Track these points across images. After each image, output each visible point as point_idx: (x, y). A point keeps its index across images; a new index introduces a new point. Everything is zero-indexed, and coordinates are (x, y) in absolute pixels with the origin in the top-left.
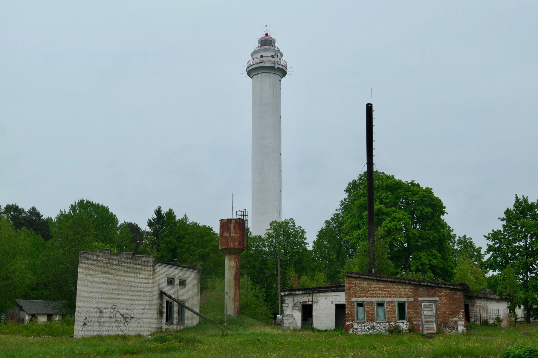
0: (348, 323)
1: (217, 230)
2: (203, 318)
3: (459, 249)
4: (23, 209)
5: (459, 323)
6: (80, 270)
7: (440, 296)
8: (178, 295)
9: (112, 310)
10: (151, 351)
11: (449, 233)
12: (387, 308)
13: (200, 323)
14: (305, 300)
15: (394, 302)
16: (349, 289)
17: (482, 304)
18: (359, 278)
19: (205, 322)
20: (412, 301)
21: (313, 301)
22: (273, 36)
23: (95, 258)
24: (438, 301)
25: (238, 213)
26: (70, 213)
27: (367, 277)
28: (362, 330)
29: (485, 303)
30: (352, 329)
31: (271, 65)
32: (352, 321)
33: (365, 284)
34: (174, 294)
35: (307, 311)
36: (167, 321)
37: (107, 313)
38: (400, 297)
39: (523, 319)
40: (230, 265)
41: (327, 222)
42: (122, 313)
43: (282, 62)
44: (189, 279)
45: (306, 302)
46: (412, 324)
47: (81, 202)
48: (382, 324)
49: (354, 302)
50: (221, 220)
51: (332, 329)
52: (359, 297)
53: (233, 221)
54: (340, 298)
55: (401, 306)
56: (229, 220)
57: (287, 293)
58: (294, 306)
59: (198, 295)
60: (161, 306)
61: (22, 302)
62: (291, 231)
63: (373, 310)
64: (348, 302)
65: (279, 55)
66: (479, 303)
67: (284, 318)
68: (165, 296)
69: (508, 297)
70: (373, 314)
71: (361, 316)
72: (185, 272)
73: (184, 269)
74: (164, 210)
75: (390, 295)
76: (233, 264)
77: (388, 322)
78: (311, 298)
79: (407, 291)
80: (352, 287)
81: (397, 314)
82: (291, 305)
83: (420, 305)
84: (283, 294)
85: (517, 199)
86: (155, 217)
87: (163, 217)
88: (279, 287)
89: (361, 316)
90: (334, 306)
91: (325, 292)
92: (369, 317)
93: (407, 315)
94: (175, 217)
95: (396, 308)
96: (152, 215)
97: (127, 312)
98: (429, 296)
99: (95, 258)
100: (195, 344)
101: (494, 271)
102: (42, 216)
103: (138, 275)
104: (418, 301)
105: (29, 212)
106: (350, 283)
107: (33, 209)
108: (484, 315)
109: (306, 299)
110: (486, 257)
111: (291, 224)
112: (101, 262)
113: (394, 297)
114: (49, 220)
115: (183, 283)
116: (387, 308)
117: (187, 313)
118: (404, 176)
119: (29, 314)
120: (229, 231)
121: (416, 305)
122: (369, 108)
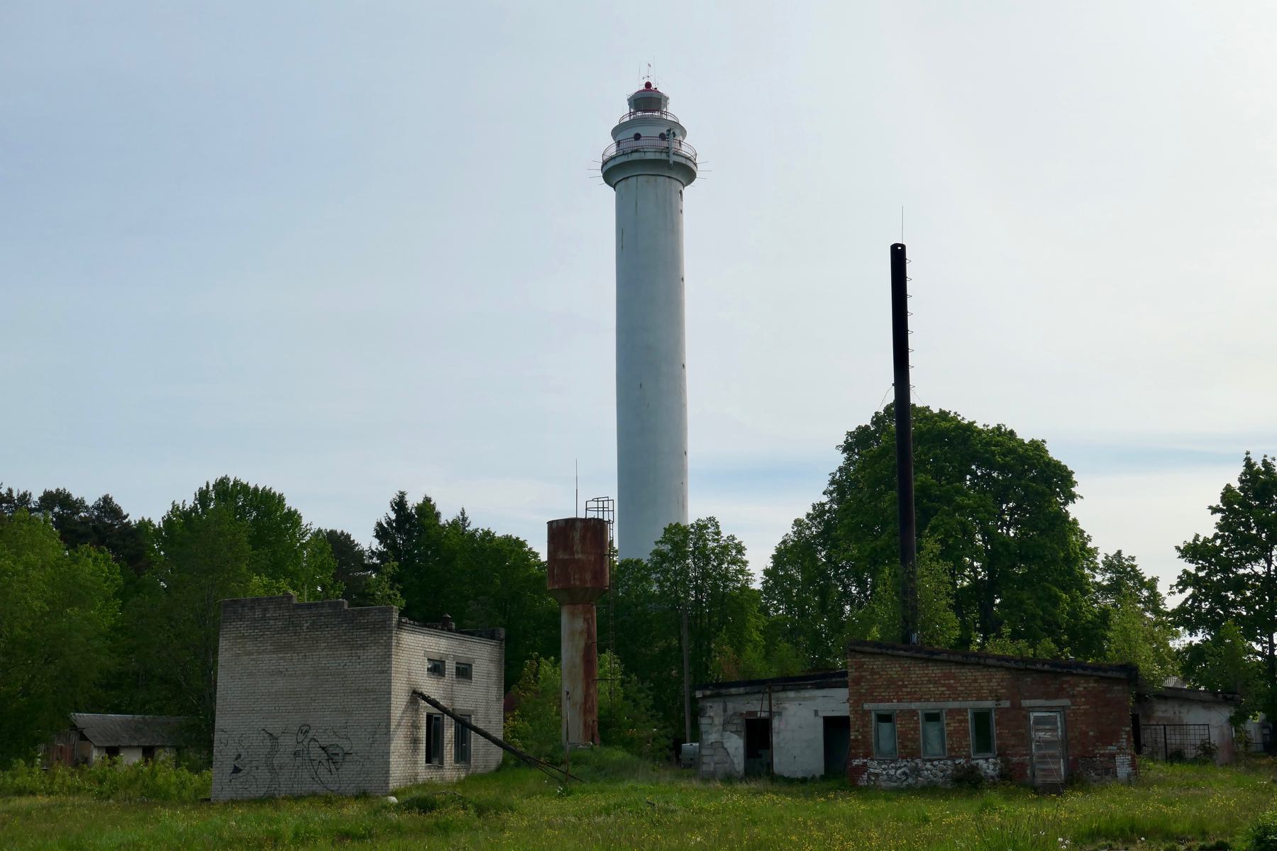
0: (856, 762)
1: (540, 547)
2: (514, 752)
3: (1105, 583)
4: (82, 502)
5: (1119, 759)
6: (223, 644)
7: (1073, 696)
8: (451, 699)
9: (301, 737)
10: (398, 830)
11: (1085, 544)
12: (948, 724)
13: (502, 767)
14: (752, 709)
15: (966, 710)
16: (858, 681)
17: (1170, 714)
18: (1001, 667)
19: (517, 758)
20: (1007, 709)
21: (770, 711)
22: (661, 87)
23: (258, 614)
24: (1068, 707)
25: (590, 505)
26: (194, 509)
27: (901, 652)
28: (890, 778)
29: (1177, 709)
30: (865, 777)
31: (658, 156)
32: (865, 756)
33: (894, 670)
34: (445, 698)
35: (758, 734)
36: (428, 760)
37: (288, 743)
38: (979, 699)
39: (1260, 747)
40: (573, 630)
41: (798, 523)
42: (324, 744)
43: (685, 150)
44: (477, 661)
45: (755, 713)
46: (1006, 762)
47: (222, 484)
48: (936, 763)
49: (870, 711)
50: (550, 524)
51: (817, 776)
52: (881, 701)
53: (579, 524)
54: (836, 702)
55: (982, 719)
56: (570, 523)
57: (708, 693)
58: (725, 724)
59: (498, 700)
60: (415, 726)
61: (83, 718)
62: (711, 545)
63: (916, 729)
64: (856, 712)
65: (677, 132)
66: (1162, 711)
67: (704, 752)
68: (423, 703)
69: (1229, 696)
70: (915, 740)
71: (886, 743)
72: (468, 644)
73: (467, 638)
74: (413, 501)
75: (956, 696)
76: (580, 624)
77: (950, 758)
78: (766, 703)
79: (994, 684)
80: (862, 677)
81: (971, 739)
82: (718, 721)
83: (1027, 718)
84: (699, 694)
85: (1249, 464)
86: (393, 516)
87: (410, 516)
88: (686, 678)
89: (886, 743)
90: (821, 721)
91: (798, 688)
92: (905, 747)
93: (996, 742)
94: (438, 515)
95: (970, 726)
96: (385, 513)
97: (335, 741)
98: (1047, 696)
99: (258, 614)
100: (504, 816)
101: (1193, 631)
102: (126, 517)
103: (360, 652)
104: (1021, 708)
105: (97, 507)
106: (860, 666)
107: (107, 500)
108: (1174, 740)
109: (756, 706)
110: (1172, 602)
111: (712, 530)
112: (272, 622)
113: (965, 699)
114: (144, 525)
115: (464, 672)
116: (950, 725)
117: (476, 742)
118: (981, 413)
119: (99, 748)
120: (568, 547)
121: (1017, 716)
122: (898, 255)
